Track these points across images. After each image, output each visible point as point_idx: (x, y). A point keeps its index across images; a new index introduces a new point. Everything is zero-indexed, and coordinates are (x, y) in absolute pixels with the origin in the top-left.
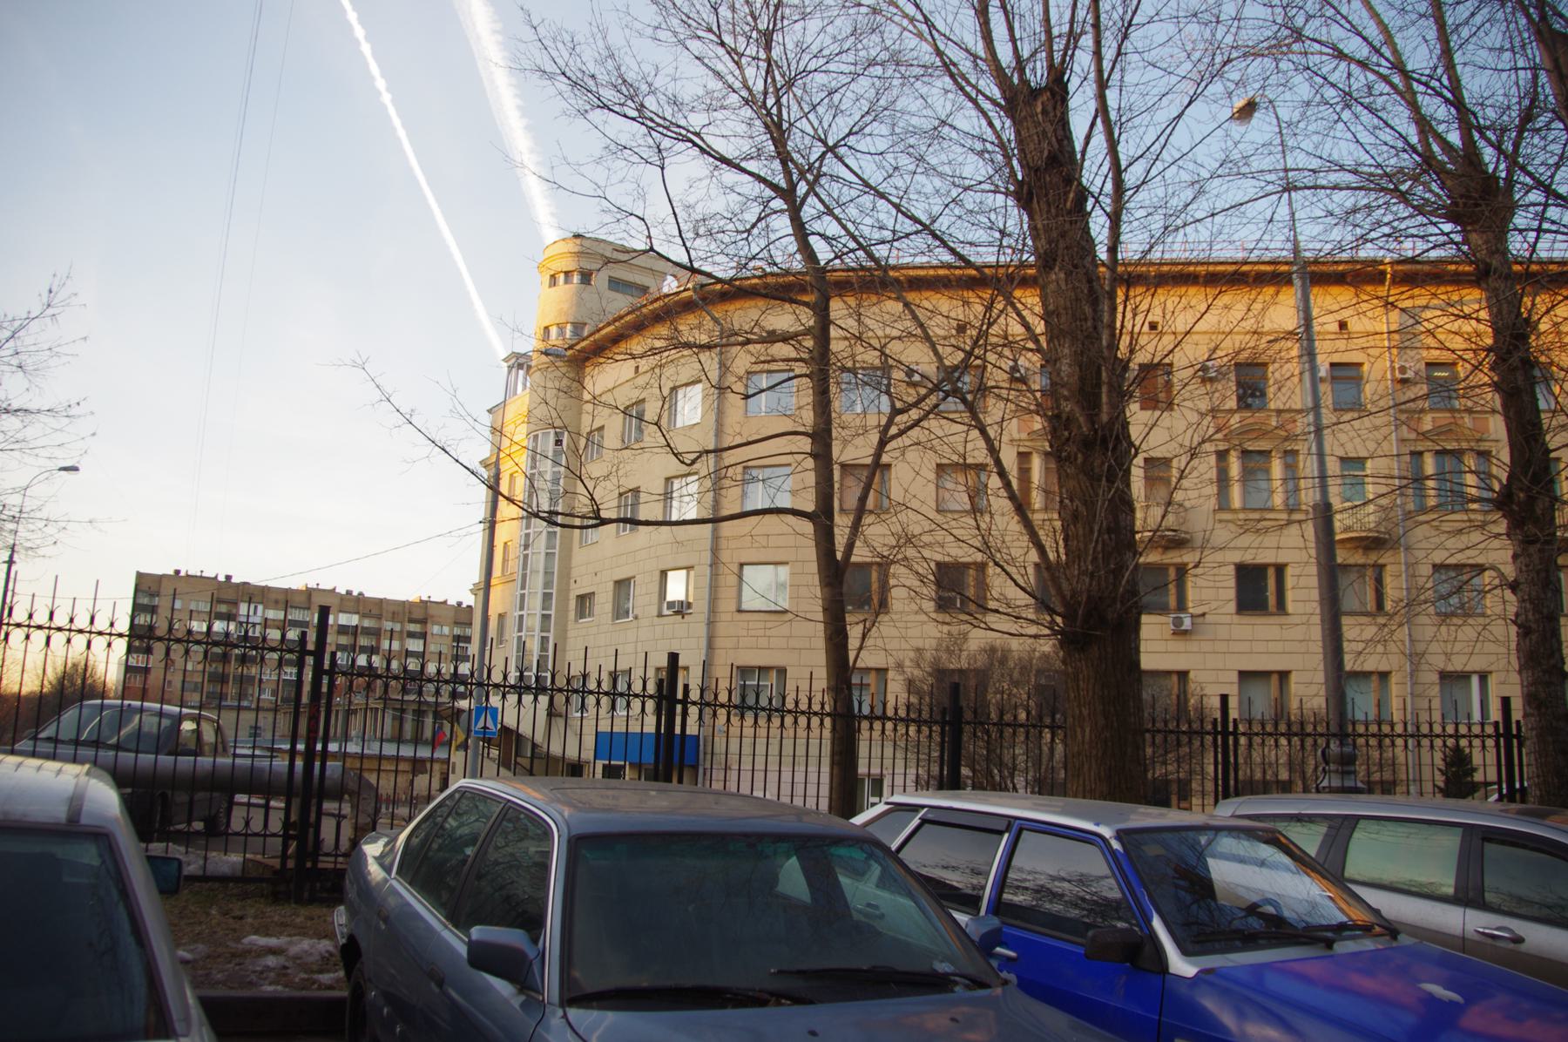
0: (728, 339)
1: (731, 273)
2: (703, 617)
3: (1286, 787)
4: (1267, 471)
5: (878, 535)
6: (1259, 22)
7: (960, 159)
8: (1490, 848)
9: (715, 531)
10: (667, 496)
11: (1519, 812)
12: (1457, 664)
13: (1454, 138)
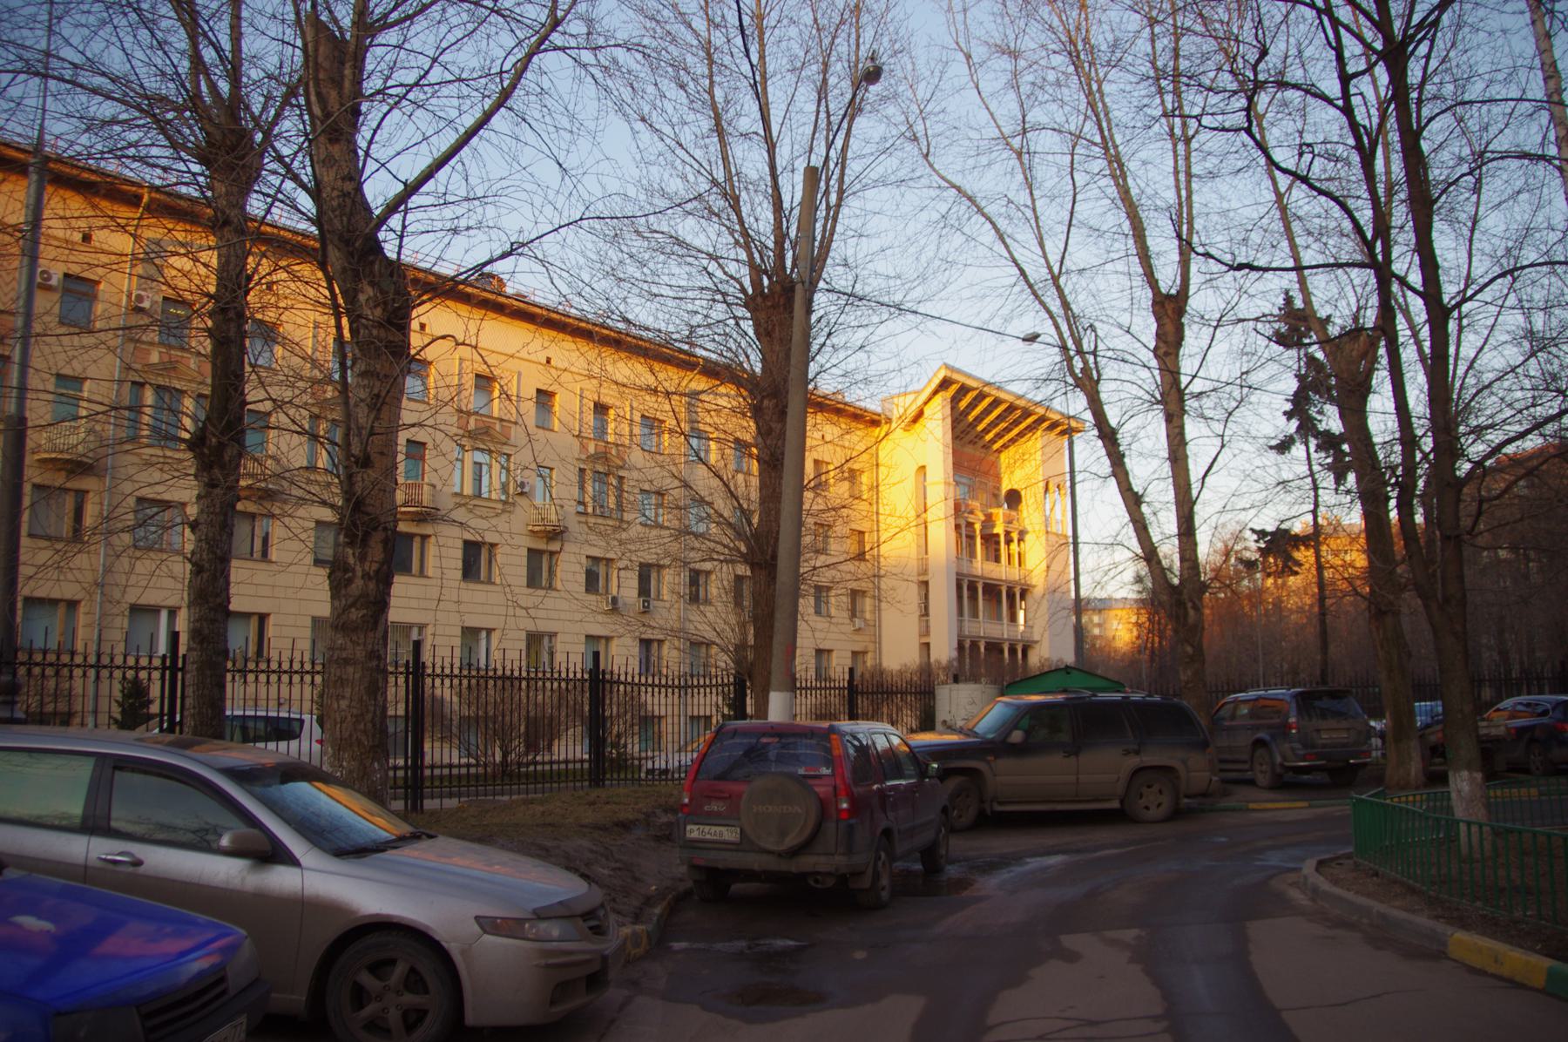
8: (119, 776)
11: (171, 744)
12: (150, 598)
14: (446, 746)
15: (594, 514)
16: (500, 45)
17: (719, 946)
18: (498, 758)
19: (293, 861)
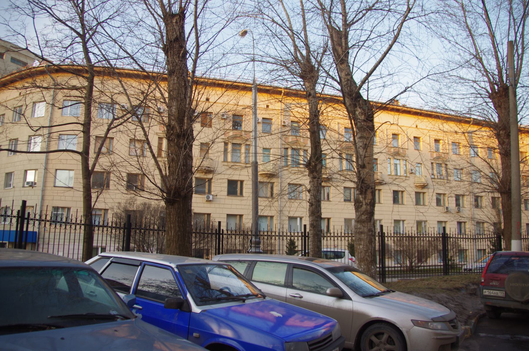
0: (57, 87)
1: (58, 63)
2: (41, 188)
3: (240, 252)
4: (240, 150)
5: (104, 162)
6: (249, 5)
7: (146, 34)
8: (295, 270)
9: (47, 157)
10: (29, 143)
11: (306, 260)
13: (304, 53)
14: (390, 260)
15: (438, 178)
16: (390, 22)
17: (499, 336)
18: (408, 265)
19: (350, 299)
